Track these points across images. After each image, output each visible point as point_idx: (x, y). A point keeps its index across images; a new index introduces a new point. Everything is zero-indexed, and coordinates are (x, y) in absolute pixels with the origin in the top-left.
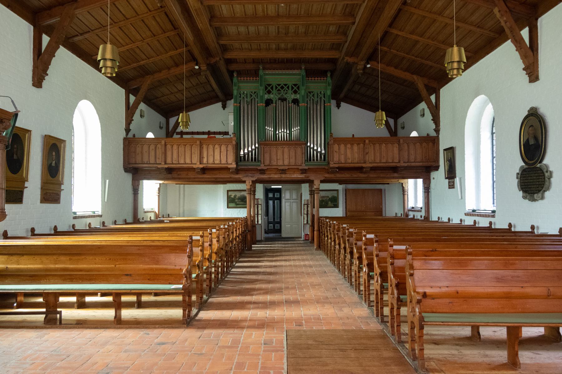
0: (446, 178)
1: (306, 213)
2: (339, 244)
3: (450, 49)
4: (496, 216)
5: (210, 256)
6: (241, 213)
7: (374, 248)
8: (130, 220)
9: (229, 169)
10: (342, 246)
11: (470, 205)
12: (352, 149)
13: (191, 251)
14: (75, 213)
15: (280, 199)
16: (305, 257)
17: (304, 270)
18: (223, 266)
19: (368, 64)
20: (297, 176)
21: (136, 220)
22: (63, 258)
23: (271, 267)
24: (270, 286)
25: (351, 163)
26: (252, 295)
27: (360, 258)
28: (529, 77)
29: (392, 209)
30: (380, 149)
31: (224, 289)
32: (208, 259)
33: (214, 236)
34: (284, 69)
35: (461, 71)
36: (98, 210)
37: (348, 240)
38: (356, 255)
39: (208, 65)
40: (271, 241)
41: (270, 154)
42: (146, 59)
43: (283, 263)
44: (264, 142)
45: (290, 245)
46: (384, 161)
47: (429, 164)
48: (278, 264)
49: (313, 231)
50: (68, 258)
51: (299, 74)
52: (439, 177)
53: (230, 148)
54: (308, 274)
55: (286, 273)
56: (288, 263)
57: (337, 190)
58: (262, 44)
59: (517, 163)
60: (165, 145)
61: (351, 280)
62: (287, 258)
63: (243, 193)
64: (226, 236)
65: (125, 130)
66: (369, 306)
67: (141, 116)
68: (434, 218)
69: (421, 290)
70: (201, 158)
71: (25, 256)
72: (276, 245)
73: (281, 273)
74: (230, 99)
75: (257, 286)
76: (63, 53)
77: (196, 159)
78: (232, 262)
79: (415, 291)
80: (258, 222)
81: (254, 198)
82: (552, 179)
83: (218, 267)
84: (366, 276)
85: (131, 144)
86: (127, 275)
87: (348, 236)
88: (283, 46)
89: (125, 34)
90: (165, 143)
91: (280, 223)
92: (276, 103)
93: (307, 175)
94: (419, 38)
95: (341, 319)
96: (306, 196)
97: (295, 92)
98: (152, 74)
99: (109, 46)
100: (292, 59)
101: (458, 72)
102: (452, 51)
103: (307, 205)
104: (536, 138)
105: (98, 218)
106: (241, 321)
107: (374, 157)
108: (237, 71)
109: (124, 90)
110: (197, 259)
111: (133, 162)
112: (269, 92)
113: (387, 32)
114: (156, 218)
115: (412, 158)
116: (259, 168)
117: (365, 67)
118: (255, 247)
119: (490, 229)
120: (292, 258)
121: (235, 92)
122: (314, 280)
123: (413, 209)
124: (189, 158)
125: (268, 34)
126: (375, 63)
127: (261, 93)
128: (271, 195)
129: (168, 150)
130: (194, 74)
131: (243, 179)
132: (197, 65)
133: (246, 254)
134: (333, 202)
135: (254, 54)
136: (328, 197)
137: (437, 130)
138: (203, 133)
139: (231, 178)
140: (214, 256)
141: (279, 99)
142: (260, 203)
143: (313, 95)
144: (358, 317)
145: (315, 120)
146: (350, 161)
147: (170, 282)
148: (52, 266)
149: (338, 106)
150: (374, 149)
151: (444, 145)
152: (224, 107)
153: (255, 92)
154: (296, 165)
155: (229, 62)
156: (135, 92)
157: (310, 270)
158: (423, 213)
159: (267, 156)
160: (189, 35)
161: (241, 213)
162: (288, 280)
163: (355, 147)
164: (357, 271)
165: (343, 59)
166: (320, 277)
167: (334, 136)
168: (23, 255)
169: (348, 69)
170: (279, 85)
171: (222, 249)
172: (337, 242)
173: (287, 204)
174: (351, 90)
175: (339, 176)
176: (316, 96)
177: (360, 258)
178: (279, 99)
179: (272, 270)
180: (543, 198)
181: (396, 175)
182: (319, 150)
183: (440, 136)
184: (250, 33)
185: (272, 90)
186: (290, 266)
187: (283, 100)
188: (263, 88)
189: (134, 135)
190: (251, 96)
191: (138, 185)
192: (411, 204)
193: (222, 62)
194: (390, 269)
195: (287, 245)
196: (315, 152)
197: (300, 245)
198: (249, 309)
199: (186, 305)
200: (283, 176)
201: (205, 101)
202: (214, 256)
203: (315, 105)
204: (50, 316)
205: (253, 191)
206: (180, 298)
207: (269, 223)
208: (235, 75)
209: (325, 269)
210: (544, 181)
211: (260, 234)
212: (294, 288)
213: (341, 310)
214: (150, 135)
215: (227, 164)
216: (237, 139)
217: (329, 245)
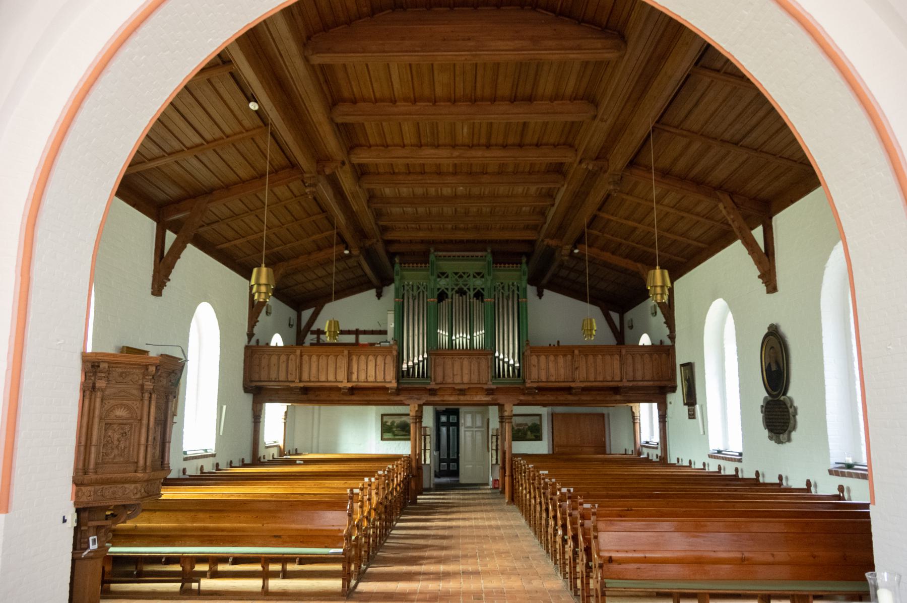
0: (685, 404)
1: (494, 448)
3: (652, 271)
4: (743, 460)
5: (369, 513)
6: (403, 448)
9: (388, 389)
11: (715, 444)
12: (556, 362)
14: (185, 453)
15: (457, 425)
16: (491, 515)
17: (488, 532)
19: (576, 248)
21: (256, 461)
22: (201, 515)
23: (444, 528)
24: (443, 553)
26: (421, 564)
28: (767, 286)
29: (619, 444)
31: (384, 557)
32: (367, 518)
33: (373, 487)
36: (211, 447)
39: (361, 248)
41: (444, 368)
43: (461, 523)
45: (471, 497)
46: (601, 379)
47: (663, 383)
48: (454, 523)
49: (504, 476)
50: (207, 515)
52: (676, 399)
53: (389, 360)
54: (494, 538)
55: (464, 537)
56: (467, 523)
57: (540, 415)
59: (761, 394)
60: (301, 356)
62: (467, 515)
63: (404, 419)
66: (565, 578)
67: (267, 313)
69: (606, 554)
70: (350, 373)
71: (157, 513)
72: (452, 497)
73: (458, 537)
74: (388, 285)
75: (427, 554)
76: (191, 252)
77: (342, 375)
79: (598, 555)
80: (425, 460)
81: (421, 427)
82: (797, 417)
85: (254, 352)
86: (275, 536)
91: (457, 461)
95: (529, 592)
96: (495, 424)
99: (264, 269)
102: (654, 274)
103: (497, 436)
104: (777, 363)
105: (211, 459)
106: (410, 593)
107: (589, 372)
110: (357, 517)
111: (256, 380)
114: (280, 456)
115: (639, 375)
116: (429, 387)
117: (572, 251)
118: (422, 499)
119: (735, 478)
122: (501, 546)
124: (331, 372)
128: (444, 419)
129: (304, 362)
130: (342, 258)
131: (406, 402)
132: (346, 249)
133: (409, 509)
135: (421, 235)
136: (526, 424)
137: (672, 337)
142: (428, 433)
144: (550, 591)
146: (553, 379)
148: (189, 525)
149: (540, 295)
151: (680, 359)
152: (379, 295)
157: (496, 533)
158: (659, 452)
160: (340, 218)
161: (403, 448)
162: (466, 546)
163: (561, 360)
165: (543, 241)
167: (531, 344)
168: (155, 511)
169: (550, 254)
171: (381, 503)
172: (533, 495)
173: (468, 434)
176: (506, 288)
180: (789, 440)
181: (618, 397)
186: (471, 527)
187: (461, 292)
189: (258, 341)
195: (466, 497)
197: (485, 496)
198: (419, 580)
199: (345, 576)
200: (462, 398)
202: (373, 513)
204: (186, 585)
205: (419, 417)
206: (339, 567)
207: (441, 461)
208: (397, 260)
209: (518, 532)
210: (789, 419)
211: (428, 479)
212: (474, 556)
213: (530, 583)
214: (277, 340)
215: (385, 382)
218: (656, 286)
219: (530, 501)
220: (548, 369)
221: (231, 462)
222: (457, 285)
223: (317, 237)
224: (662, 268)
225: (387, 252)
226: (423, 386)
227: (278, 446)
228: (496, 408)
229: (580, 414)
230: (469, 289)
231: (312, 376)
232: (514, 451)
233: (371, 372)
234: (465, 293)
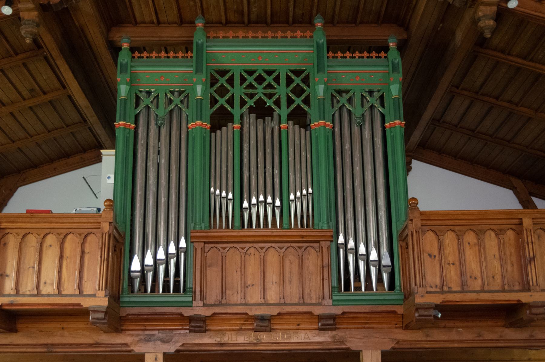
12: (480, 245)
25: (483, 291)
80: (529, 255)
93: (340, 334)
116: (188, 312)
139: (97, 344)
143: (350, 101)
145: (358, 169)
146: (477, 285)
154: (304, 304)
159: (213, 275)
163: (491, 242)
170: (250, 73)
176: (357, 100)
182: (374, 256)
187: (262, 111)
188: (203, 77)
190: (171, 101)
196: (361, 264)
200: (264, 337)
203: (356, 129)
222: (251, 96)
230: (277, 103)
233: (50, 273)
234: (270, 112)
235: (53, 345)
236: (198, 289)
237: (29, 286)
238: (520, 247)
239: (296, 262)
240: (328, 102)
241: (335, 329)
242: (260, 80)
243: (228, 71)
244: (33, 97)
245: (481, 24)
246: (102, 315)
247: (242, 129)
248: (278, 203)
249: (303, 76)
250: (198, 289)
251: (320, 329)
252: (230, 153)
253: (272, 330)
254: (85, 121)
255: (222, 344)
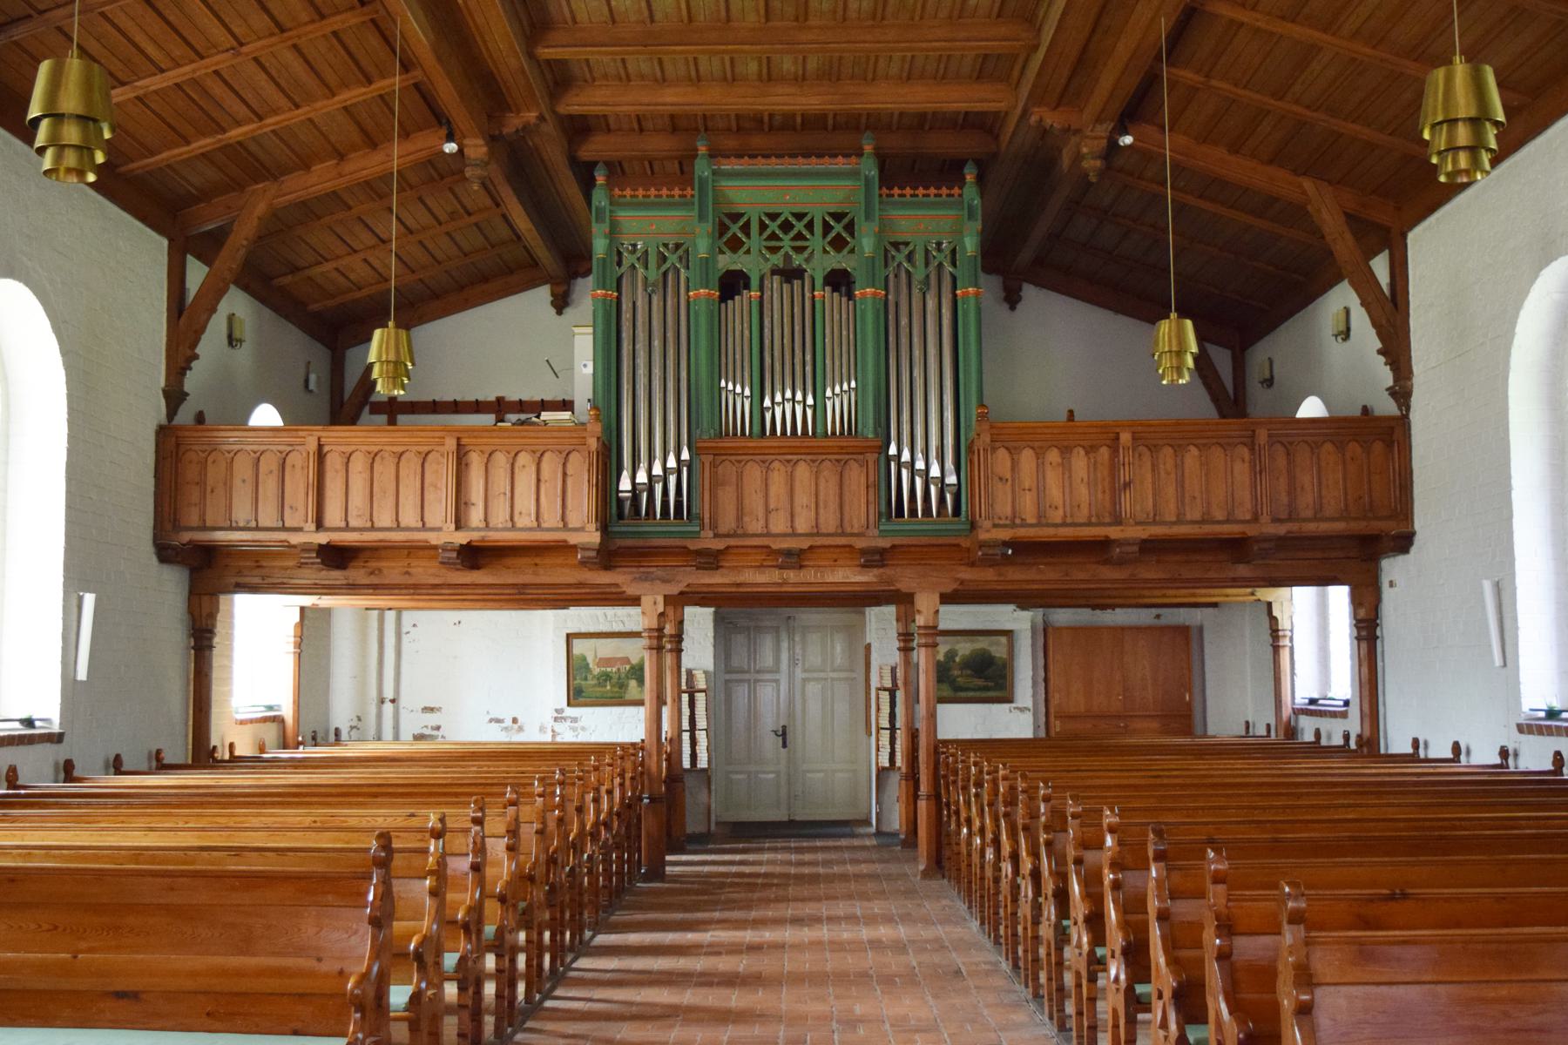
1: (885, 723)
2: (1015, 858)
3: (1440, 74)
5: (477, 910)
7: (1152, 884)
8: (177, 751)
10: (1027, 865)
12: (1066, 466)
13: (386, 895)
16: (877, 907)
18: (534, 949)
20: (848, 576)
21: (203, 755)
23: (735, 949)
25: (1064, 524)
27: (1095, 921)
29: (1233, 708)
30: (1179, 466)
32: (466, 927)
34: (793, 156)
35: (1485, 158)
36: (48, 709)
37: (1049, 844)
38: (1079, 909)
39: (493, 139)
40: (749, 839)
42: (250, 121)
43: (787, 934)
44: (716, 446)
45: (820, 856)
48: (768, 935)
51: (854, 174)
54: (888, 981)
55: (797, 979)
56: (807, 934)
57: (1008, 633)
58: (703, 59)
61: (1061, 1010)
62: (808, 909)
64: (552, 825)
65: (166, 394)
68: (1397, 742)
72: (766, 857)
77: (439, 511)
78: (578, 931)
80: (694, 756)
83: (515, 950)
84: (1121, 997)
85: (182, 454)
86: (120, 995)
87: (1047, 828)
88: (787, 65)
89: (168, 23)
90: (320, 446)
92: (761, 289)
93: (888, 571)
94: (1317, 34)
97: (838, 244)
98: (276, 179)
99: (74, 64)
100: (824, 116)
101: (1476, 164)
102: (1449, 80)
108: (609, 165)
109: (165, 242)
110: (414, 928)
112: (735, 245)
113: (1194, 9)
116: (693, 545)
117: (1113, 145)
118: (679, 864)
120: (824, 909)
121: (600, 246)
123: (1314, 708)
125: (728, 20)
126: (1149, 130)
127: (702, 247)
131: (631, 590)
132: (450, 138)
134: (984, 677)
135: (673, 98)
137: (1401, 393)
138: (477, 407)
140: (492, 909)
141: (774, 272)
143: (910, 258)
145: (917, 353)
146: (1057, 517)
147: (299, 1025)
149: (1012, 299)
150: (1154, 468)
152: (561, 303)
153: (678, 246)
154: (843, 534)
155: (579, 128)
156: (208, 246)
158: (1354, 725)
159: (727, 497)
161: (620, 725)
163: (1080, 462)
164: (1084, 974)
166: (935, 997)
170: (773, 217)
171: (531, 879)
172: (1006, 848)
174: (1053, 237)
175: (1018, 575)
176: (919, 257)
177: (1095, 921)
178: (774, 272)
179: (741, 964)
181: (1242, 570)
182: (935, 471)
183: (1416, 417)
184: (658, 16)
185: (748, 235)
186: (817, 945)
187: (791, 274)
188: (708, 227)
190: (664, 259)
191: (212, 616)
192: (1303, 686)
193: (549, 128)
194: (1214, 974)
195: (807, 857)
196: (919, 482)
197: (860, 855)
200: (792, 576)
201: (485, 279)
202: (492, 909)
205: (666, 640)
208: (600, 179)
216: (607, 429)
217: (976, 858)
218: (1452, 122)
219: (997, 869)
220: (1040, 489)
221: (118, 758)
223: (355, 94)
224: (1474, 57)
225: (574, 162)
226: (678, 542)
227: (279, 720)
228: (890, 611)
229: (1123, 629)
231: (353, 512)
232: (944, 733)
233: (525, 502)
235: (525, 586)
236: (707, 516)
237: (500, 516)
238: (1113, 468)
239: (834, 480)
240: (880, 262)
241: (883, 566)
242: (786, 226)
243: (742, 215)
244: (453, 219)
245: (1085, 164)
246: (593, 554)
247: (761, 297)
248: (810, 401)
249: (846, 221)
250: (707, 516)
251: (863, 566)
252: (746, 333)
253: (801, 567)
254: (519, 238)
255: (739, 585)
